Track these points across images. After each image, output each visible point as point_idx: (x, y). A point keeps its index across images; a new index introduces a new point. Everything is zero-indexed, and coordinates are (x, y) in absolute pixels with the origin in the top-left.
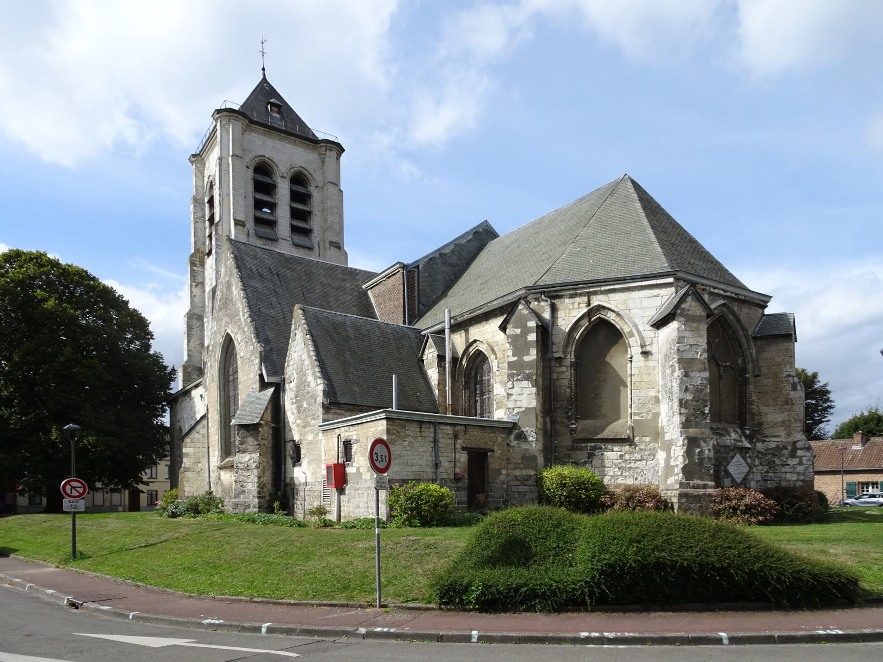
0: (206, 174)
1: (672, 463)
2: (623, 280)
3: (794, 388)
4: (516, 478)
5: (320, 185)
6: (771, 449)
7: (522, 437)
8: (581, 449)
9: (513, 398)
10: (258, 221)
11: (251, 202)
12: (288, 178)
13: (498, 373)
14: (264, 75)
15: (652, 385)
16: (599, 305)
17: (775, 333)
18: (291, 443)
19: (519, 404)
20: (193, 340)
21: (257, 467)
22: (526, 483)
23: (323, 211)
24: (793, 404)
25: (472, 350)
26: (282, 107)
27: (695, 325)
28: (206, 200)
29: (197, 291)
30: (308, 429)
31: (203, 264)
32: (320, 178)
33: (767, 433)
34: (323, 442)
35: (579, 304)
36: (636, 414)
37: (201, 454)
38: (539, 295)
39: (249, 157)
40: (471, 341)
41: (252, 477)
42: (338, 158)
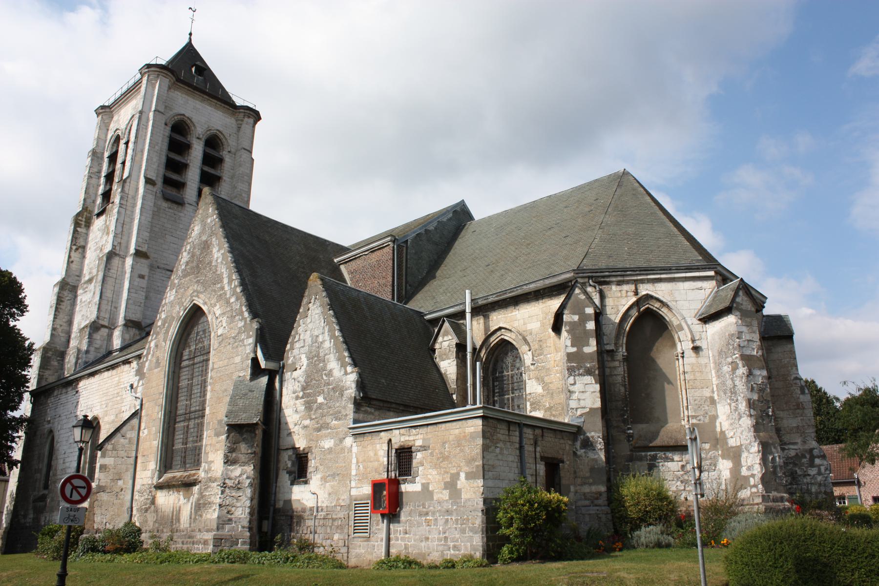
0: (113, 126)
1: (744, 472)
2: (668, 270)
3: (803, 392)
4: (585, 496)
5: (233, 150)
6: (791, 458)
7: (588, 444)
8: (641, 459)
9: (575, 396)
10: (167, 181)
11: (164, 159)
12: (203, 140)
13: (532, 367)
14: (190, 39)
15: (707, 384)
16: (647, 295)
17: (779, 333)
18: (290, 452)
19: (582, 403)
20: (61, 316)
21: (251, 485)
22: (596, 502)
23: (232, 177)
24: (804, 408)
25: (494, 340)
26: (203, 70)
27: (748, 320)
28: (107, 154)
29: (75, 256)
30: (324, 432)
31: (88, 224)
32: (234, 144)
33: (785, 440)
34: (355, 449)
35: (627, 292)
36: (693, 417)
37: (124, 467)
38: (586, 280)
39: (171, 113)
40: (492, 329)
41: (244, 499)
42: (255, 123)
